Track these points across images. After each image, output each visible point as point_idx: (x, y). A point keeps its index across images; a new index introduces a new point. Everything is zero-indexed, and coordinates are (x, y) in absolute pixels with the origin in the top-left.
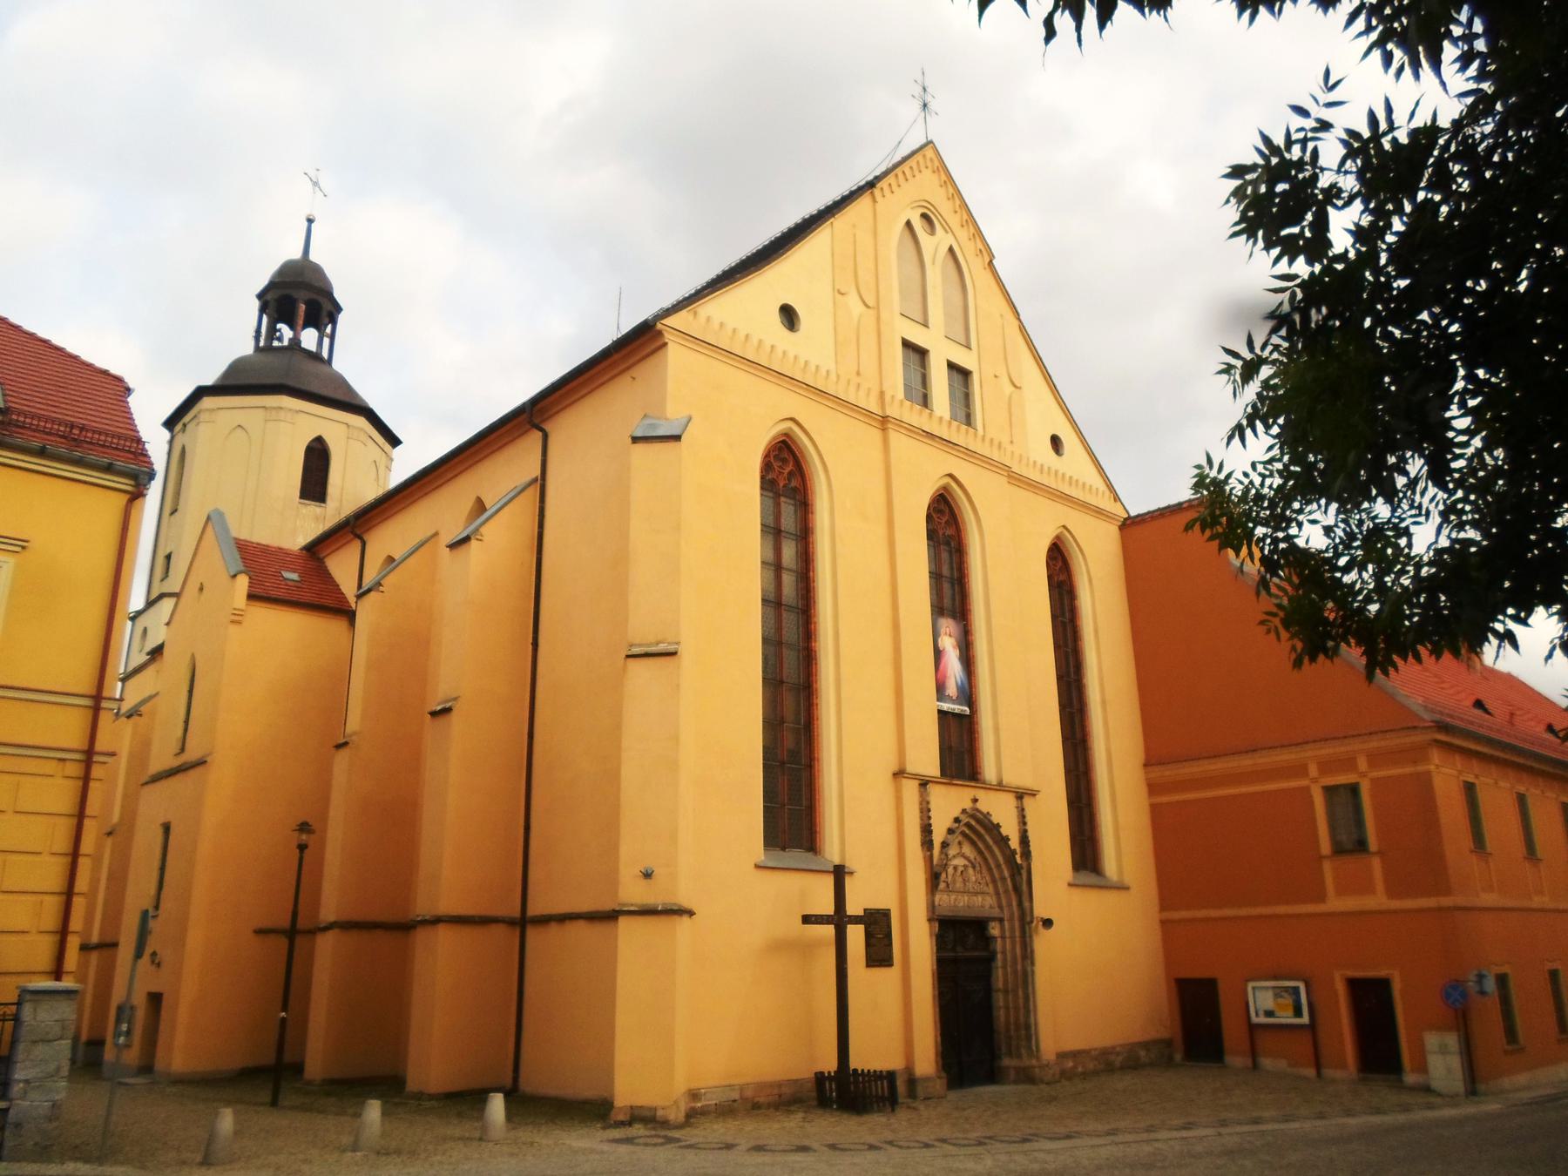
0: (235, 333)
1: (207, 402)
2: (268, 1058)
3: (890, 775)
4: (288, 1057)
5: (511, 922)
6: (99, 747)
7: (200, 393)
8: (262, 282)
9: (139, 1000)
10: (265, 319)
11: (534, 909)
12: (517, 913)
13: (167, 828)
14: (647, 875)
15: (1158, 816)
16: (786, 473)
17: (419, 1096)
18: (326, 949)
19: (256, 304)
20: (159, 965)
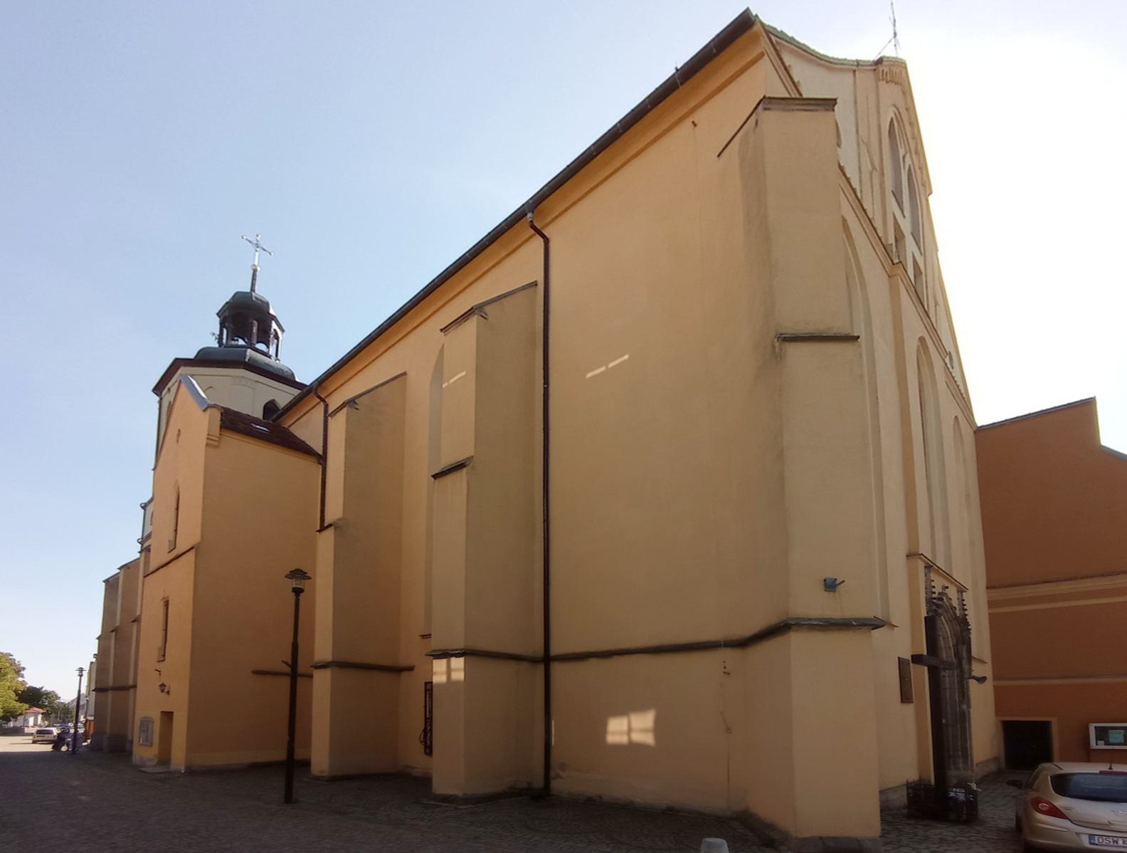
0: (204, 333)
1: (182, 370)
2: (281, 755)
3: (905, 555)
4: (299, 755)
5: (533, 661)
6: (286, 682)
7: (178, 363)
8: (220, 305)
9: (156, 717)
10: (225, 331)
11: (556, 649)
12: (539, 650)
13: (167, 604)
14: (831, 586)
15: (992, 618)
16: (904, 217)
17: (446, 799)
18: (322, 683)
19: (217, 320)
20: (168, 692)
